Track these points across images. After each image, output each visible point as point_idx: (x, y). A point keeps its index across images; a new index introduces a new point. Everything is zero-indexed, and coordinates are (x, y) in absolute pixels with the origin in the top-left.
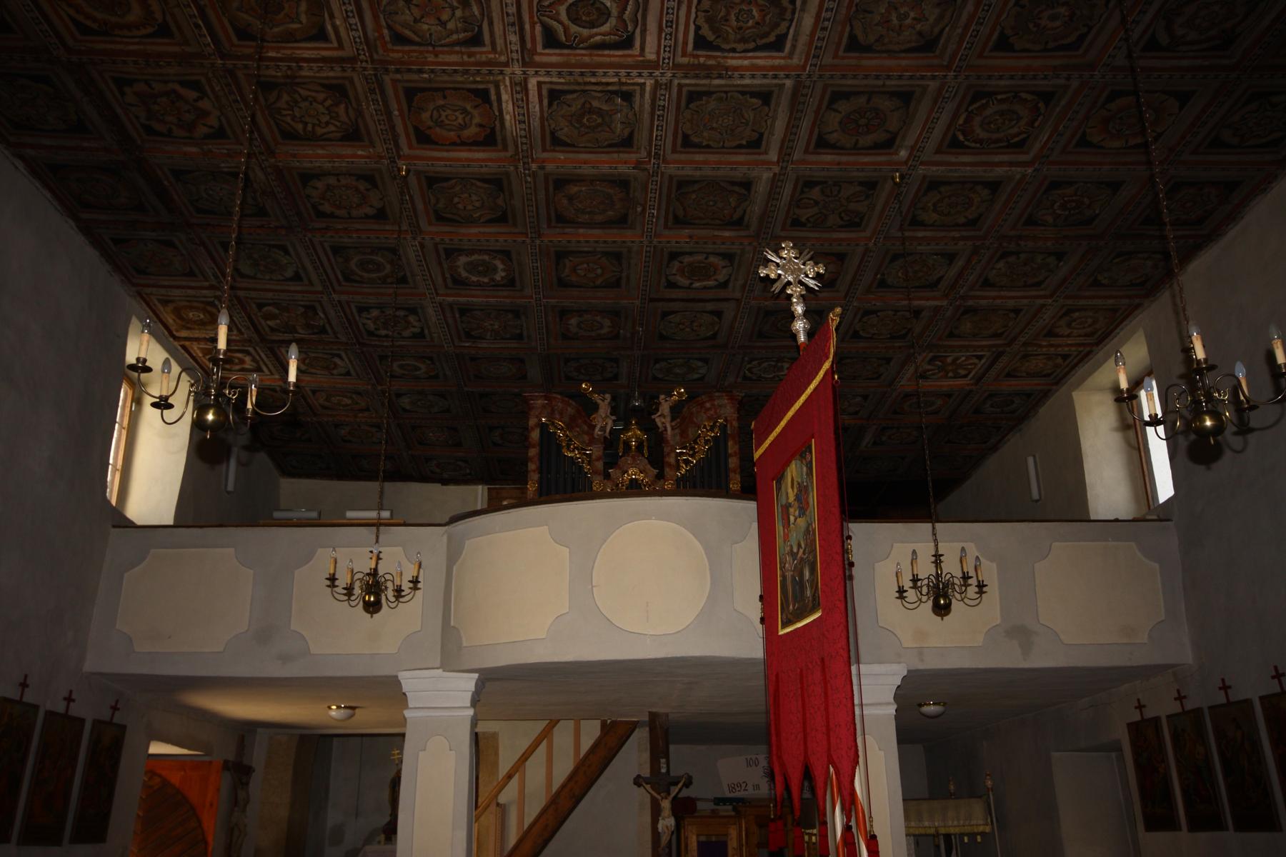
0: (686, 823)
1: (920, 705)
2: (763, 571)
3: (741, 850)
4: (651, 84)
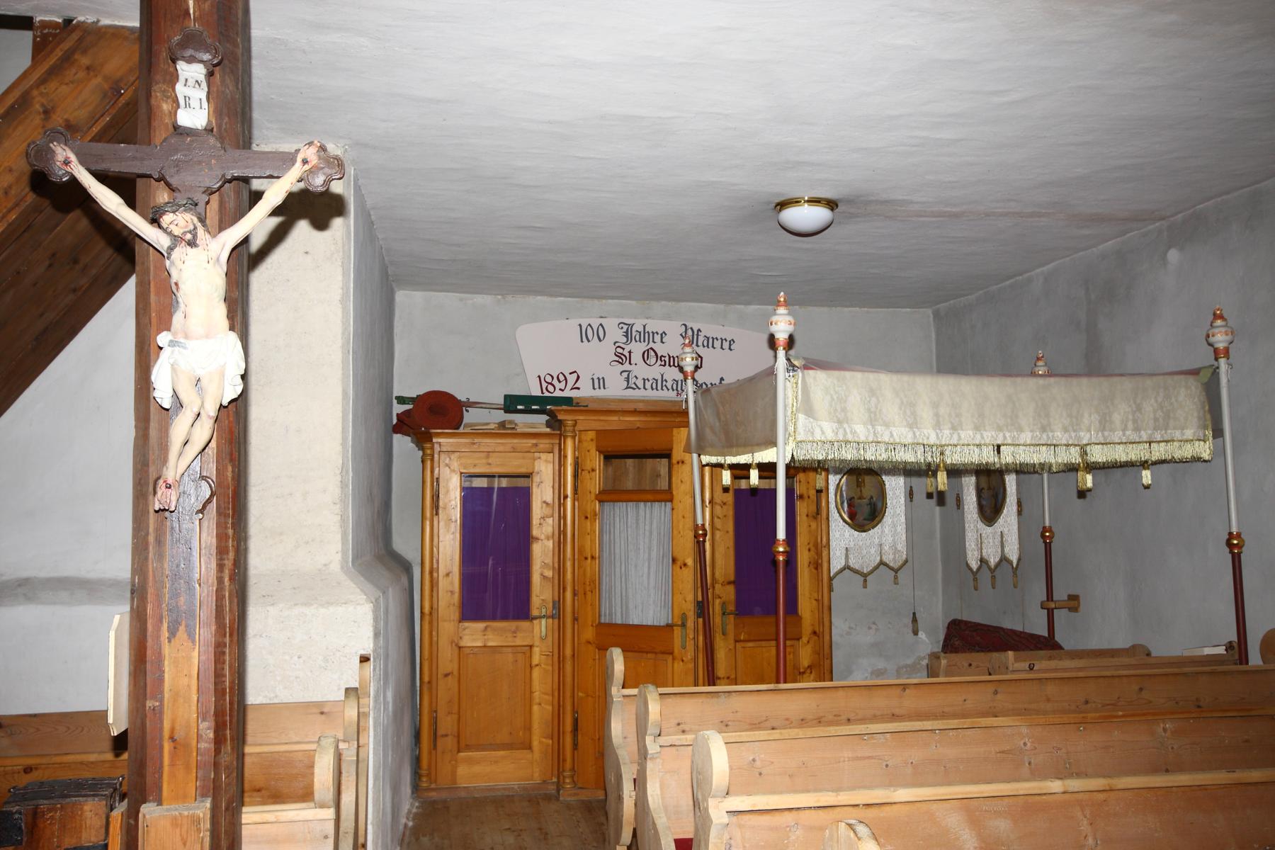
0: (437, 448)
1: (783, 205)
2: (463, 530)
3: (562, 505)
4: (1016, 660)
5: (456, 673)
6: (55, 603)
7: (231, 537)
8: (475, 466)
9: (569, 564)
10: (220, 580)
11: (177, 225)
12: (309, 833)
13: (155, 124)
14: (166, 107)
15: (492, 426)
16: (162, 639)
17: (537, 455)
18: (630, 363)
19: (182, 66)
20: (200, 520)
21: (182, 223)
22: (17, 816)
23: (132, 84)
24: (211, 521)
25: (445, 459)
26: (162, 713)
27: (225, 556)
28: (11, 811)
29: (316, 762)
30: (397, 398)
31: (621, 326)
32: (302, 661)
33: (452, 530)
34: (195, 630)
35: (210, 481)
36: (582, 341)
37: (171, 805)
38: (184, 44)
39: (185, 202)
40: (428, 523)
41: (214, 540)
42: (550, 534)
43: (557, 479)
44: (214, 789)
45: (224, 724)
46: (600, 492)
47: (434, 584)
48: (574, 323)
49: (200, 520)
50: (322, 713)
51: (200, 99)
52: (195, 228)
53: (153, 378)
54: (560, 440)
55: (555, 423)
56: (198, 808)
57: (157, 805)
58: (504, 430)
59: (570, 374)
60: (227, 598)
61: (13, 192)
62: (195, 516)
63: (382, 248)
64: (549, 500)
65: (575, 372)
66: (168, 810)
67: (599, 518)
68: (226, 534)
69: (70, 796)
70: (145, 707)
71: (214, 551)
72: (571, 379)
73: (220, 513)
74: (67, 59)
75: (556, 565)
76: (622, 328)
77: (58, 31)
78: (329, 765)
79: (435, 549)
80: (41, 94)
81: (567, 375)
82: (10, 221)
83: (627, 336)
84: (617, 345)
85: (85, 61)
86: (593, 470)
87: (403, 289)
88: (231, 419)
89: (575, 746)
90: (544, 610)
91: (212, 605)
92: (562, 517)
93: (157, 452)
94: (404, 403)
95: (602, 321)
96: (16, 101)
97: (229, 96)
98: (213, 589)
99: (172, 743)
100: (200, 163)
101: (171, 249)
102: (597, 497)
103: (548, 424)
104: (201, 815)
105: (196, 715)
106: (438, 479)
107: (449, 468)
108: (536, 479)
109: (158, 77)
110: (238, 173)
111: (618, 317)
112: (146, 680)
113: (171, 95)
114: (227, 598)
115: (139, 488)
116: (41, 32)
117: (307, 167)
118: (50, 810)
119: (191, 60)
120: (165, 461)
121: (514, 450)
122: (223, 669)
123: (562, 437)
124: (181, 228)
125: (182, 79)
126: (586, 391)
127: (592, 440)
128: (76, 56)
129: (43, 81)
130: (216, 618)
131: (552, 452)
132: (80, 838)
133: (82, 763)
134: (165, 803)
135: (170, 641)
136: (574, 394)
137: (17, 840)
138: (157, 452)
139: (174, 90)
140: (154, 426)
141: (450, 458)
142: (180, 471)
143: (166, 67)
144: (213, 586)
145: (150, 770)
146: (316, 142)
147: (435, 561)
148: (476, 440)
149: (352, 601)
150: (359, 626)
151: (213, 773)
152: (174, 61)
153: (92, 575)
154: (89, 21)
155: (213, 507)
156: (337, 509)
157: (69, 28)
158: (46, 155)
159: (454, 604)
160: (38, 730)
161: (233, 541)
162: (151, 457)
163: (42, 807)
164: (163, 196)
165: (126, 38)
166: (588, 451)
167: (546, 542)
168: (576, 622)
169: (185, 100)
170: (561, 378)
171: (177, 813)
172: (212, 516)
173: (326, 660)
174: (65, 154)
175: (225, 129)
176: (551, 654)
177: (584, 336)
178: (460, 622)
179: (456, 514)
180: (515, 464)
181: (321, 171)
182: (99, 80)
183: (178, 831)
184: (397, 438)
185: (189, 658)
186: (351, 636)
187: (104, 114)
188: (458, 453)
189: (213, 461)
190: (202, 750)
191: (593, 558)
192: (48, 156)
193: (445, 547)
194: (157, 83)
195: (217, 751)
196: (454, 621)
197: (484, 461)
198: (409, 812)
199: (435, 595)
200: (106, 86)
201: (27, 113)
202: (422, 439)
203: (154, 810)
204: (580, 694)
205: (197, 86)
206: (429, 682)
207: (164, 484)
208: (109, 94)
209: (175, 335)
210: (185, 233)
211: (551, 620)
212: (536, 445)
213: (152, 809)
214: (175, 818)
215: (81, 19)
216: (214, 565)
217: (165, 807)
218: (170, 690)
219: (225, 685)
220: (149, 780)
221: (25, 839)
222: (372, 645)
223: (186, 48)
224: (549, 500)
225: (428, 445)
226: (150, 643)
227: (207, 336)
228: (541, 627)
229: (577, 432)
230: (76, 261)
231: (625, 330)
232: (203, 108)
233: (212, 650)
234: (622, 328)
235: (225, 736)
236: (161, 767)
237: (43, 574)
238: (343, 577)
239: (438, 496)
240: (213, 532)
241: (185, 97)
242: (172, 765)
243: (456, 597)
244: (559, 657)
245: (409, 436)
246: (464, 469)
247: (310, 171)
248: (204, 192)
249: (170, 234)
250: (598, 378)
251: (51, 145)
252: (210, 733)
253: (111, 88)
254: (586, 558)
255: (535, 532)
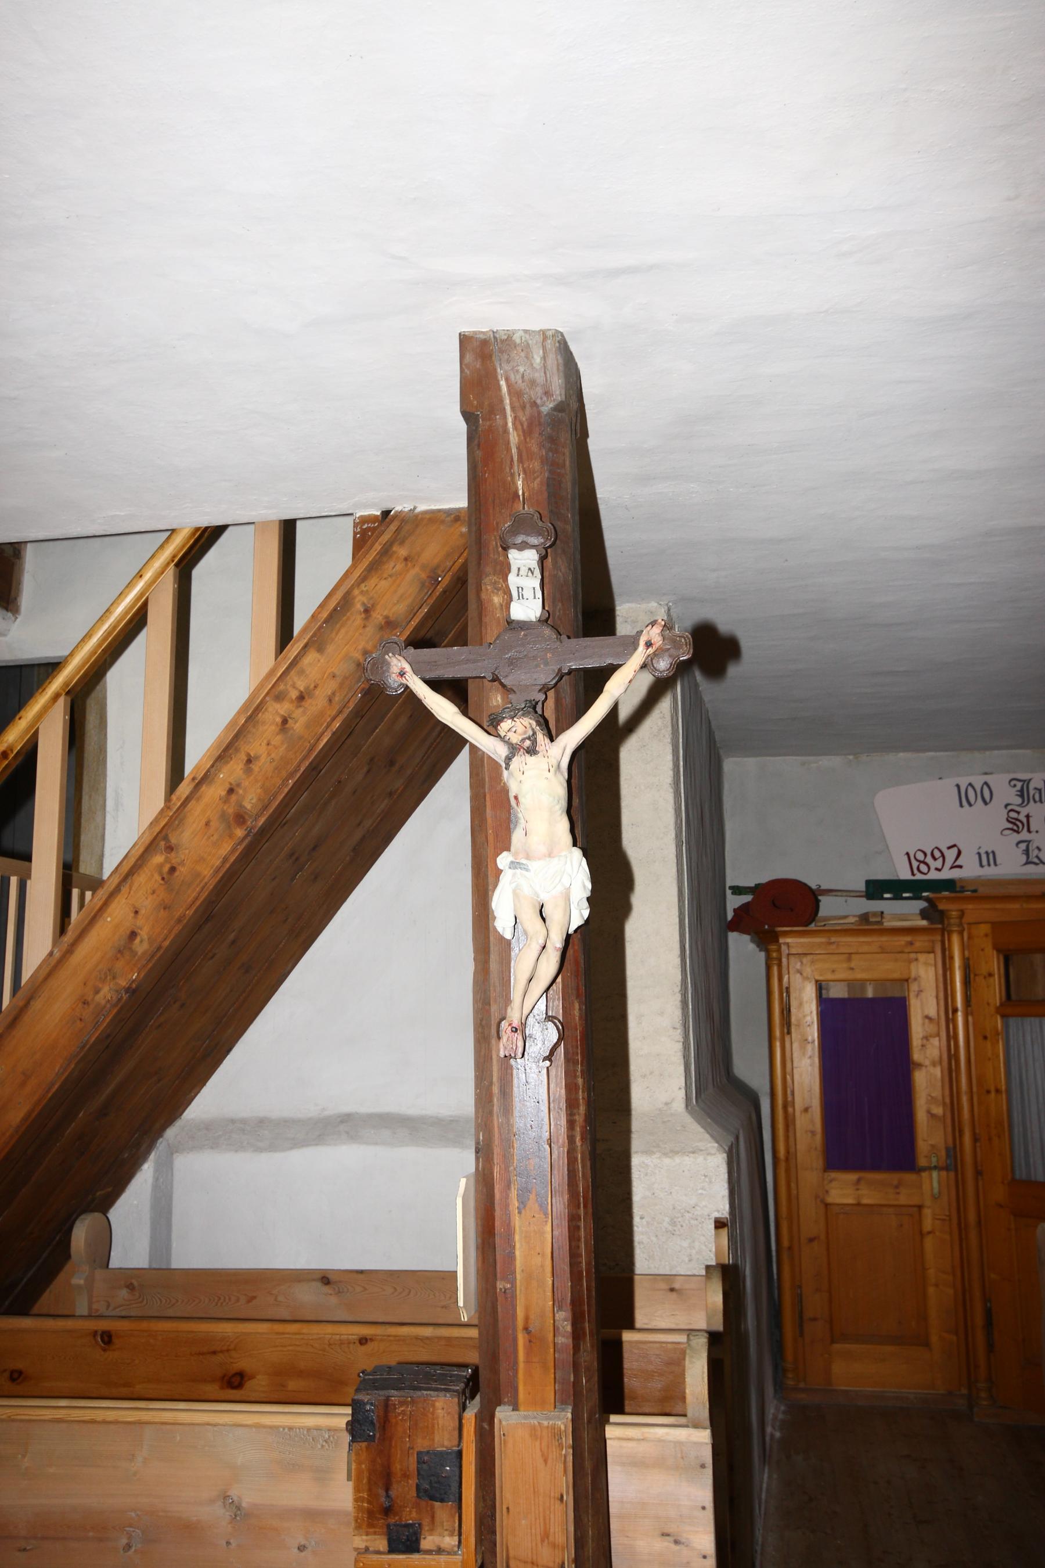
3: (950, 1020)
5: (823, 1237)
6: (376, 1144)
7: (581, 1087)
8: (833, 971)
9: (965, 1099)
10: (571, 1139)
11: (515, 732)
12: (682, 1458)
13: (486, 620)
14: (497, 600)
15: (852, 920)
16: (511, 1208)
17: (913, 956)
18: (1029, 831)
19: (513, 555)
20: (548, 1068)
21: (520, 729)
22: (368, 1407)
23: (450, 570)
24: (559, 1069)
25: (796, 964)
26: (514, 1297)
27: (575, 1111)
28: (362, 1401)
29: (687, 1368)
30: (731, 888)
31: (1013, 783)
32: (645, 1223)
33: (809, 1052)
34: (547, 1200)
35: (557, 1021)
36: (961, 806)
37: (528, 1411)
38: (515, 531)
39: (523, 706)
40: (778, 1044)
41: (563, 1091)
42: (937, 1058)
43: (941, 986)
44: (574, 1395)
45: (582, 1313)
46: (1002, 1004)
47: (790, 1122)
48: (949, 783)
49: (548, 1068)
50: (672, 1290)
51: (534, 588)
52: (534, 733)
53: (494, 905)
54: (943, 935)
55: (932, 913)
56: (559, 1418)
57: (513, 1410)
58: (868, 925)
59: (949, 848)
60: (579, 1161)
61: (337, 699)
62: (541, 1064)
63: (708, 711)
64: (932, 1012)
65: (954, 846)
66: (526, 1417)
67: (1002, 1038)
68: (576, 1084)
69: (420, 1389)
70: (496, 1288)
71: (563, 1105)
72: (950, 855)
73: (568, 1059)
74: (386, 552)
75: (948, 1100)
76: (1015, 786)
77: (376, 524)
78: (703, 1373)
79: (788, 1077)
80: (362, 592)
81: (944, 850)
82: (334, 730)
83: (1022, 796)
84: (1009, 808)
85: (402, 552)
86: (991, 975)
87: (733, 757)
88: (576, 947)
89: (990, 1347)
90: (934, 1160)
91: (563, 1169)
92: (951, 1037)
93: (498, 989)
94: (740, 894)
95: (987, 778)
96: (338, 604)
97: (562, 579)
98: (564, 1151)
99: (526, 1335)
100: (535, 658)
101: (508, 759)
102: (998, 1010)
103: (924, 914)
104: (563, 1427)
105: (551, 1303)
106: (788, 989)
107: (801, 974)
108: (914, 987)
109: (488, 569)
110: (576, 665)
111: (1008, 772)
112: (495, 1255)
113: (502, 586)
114: (579, 1161)
115: (480, 1030)
116: (361, 528)
117: (651, 651)
118: (402, 1403)
119: (523, 547)
120: (507, 1001)
121: (883, 950)
122: (578, 1247)
123: (945, 932)
124: (521, 735)
125: (514, 569)
126: (970, 870)
127: (986, 935)
128: (394, 549)
129: (363, 579)
130: (569, 1185)
131: (933, 952)
132: (433, 1440)
133: (417, 1338)
134: (521, 1408)
135: (520, 1213)
136: (955, 874)
137: (369, 1436)
138: (498, 989)
139: (506, 580)
140: (494, 957)
141: (802, 963)
142: (526, 1012)
143: (496, 556)
144: (563, 1147)
145: (503, 1366)
146: (660, 621)
147: (789, 1092)
148: (833, 940)
149: (701, 1150)
150: (711, 1182)
151: (572, 1376)
152: (506, 549)
153: (412, 1112)
154: (406, 510)
155: (561, 1052)
156: (678, 1035)
157: (387, 520)
158: (382, 668)
159: (816, 1149)
160: (365, 1289)
161: (583, 1092)
162: (493, 995)
163: (393, 1398)
164: (497, 699)
165: (443, 522)
166: (983, 950)
167: (931, 1069)
168: (980, 1178)
169: (518, 591)
170: (937, 854)
171: (536, 1422)
172: (560, 1063)
173: (673, 1223)
174: (400, 664)
175: (559, 616)
176: (948, 1218)
177: (964, 799)
178: (825, 1171)
179: (813, 1033)
180: (888, 968)
181: (667, 654)
182: (417, 569)
183: (538, 1443)
184: (733, 937)
185: (542, 1233)
186: (701, 1194)
187: (422, 605)
188: (812, 956)
189: (559, 998)
190: (559, 1346)
191: (998, 1091)
192: (384, 668)
193: (801, 1076)
194: (487, 576)
195: (576, 1348)
196: (817, 1169)
197: (845, 965)
198: (775, 1418)
199: (791, 1134)
200: (423, 576)
201: (348, 614)
202: (766, 939)
203: (510, 1416)
204: (993, 1276)
205: (530, 574)
206: (790, 1248)
207: (510, 1028)
208: (427, 584)
209: (516, 855)
210: (523, 740)
211: (944, 1173)
212: (911, 943)
213: (508, 1413)
214: (533, 1428)
215: (398, 508)
216: (563, 1122)
217: (522, 1413)
218: (523, 1271)
219: (582, 1268)
220: (503, 1376)
221: (378, 1435)
222: (727, 1207)
223: (517, 534)
224: (932, 1012)
225: (773, 947)
226: (498, 1212)
227: (550, 855)
228: (933, 1182)
229: (966, 926)
230: (392, 763)
231: (1019, 787)
232: (537, 597)
233: (565, 1224)
234: (1015, 786)
235: (583, 1329)
236: (516, 1363)
237: (364, 1109)
238: (689, 1120)
239: (790, 1010)
240: (562, 1082)
241: (518, 588)
242: (528, 1361)
243: (819, 1138)
244: (959, 1224)
245: (749, 934)
246: (821, 975)
247: (655, 654)
248: (540, 691)
249: (508, 743)
250: (987, 853)
251: (387, 657)
252: (567, 1325)
253: (428, 577)
254: (988, 1092)
255: (917, 1056)
